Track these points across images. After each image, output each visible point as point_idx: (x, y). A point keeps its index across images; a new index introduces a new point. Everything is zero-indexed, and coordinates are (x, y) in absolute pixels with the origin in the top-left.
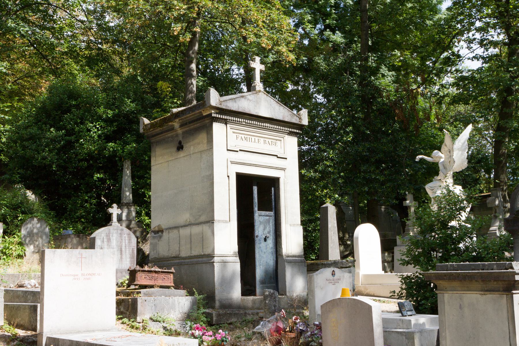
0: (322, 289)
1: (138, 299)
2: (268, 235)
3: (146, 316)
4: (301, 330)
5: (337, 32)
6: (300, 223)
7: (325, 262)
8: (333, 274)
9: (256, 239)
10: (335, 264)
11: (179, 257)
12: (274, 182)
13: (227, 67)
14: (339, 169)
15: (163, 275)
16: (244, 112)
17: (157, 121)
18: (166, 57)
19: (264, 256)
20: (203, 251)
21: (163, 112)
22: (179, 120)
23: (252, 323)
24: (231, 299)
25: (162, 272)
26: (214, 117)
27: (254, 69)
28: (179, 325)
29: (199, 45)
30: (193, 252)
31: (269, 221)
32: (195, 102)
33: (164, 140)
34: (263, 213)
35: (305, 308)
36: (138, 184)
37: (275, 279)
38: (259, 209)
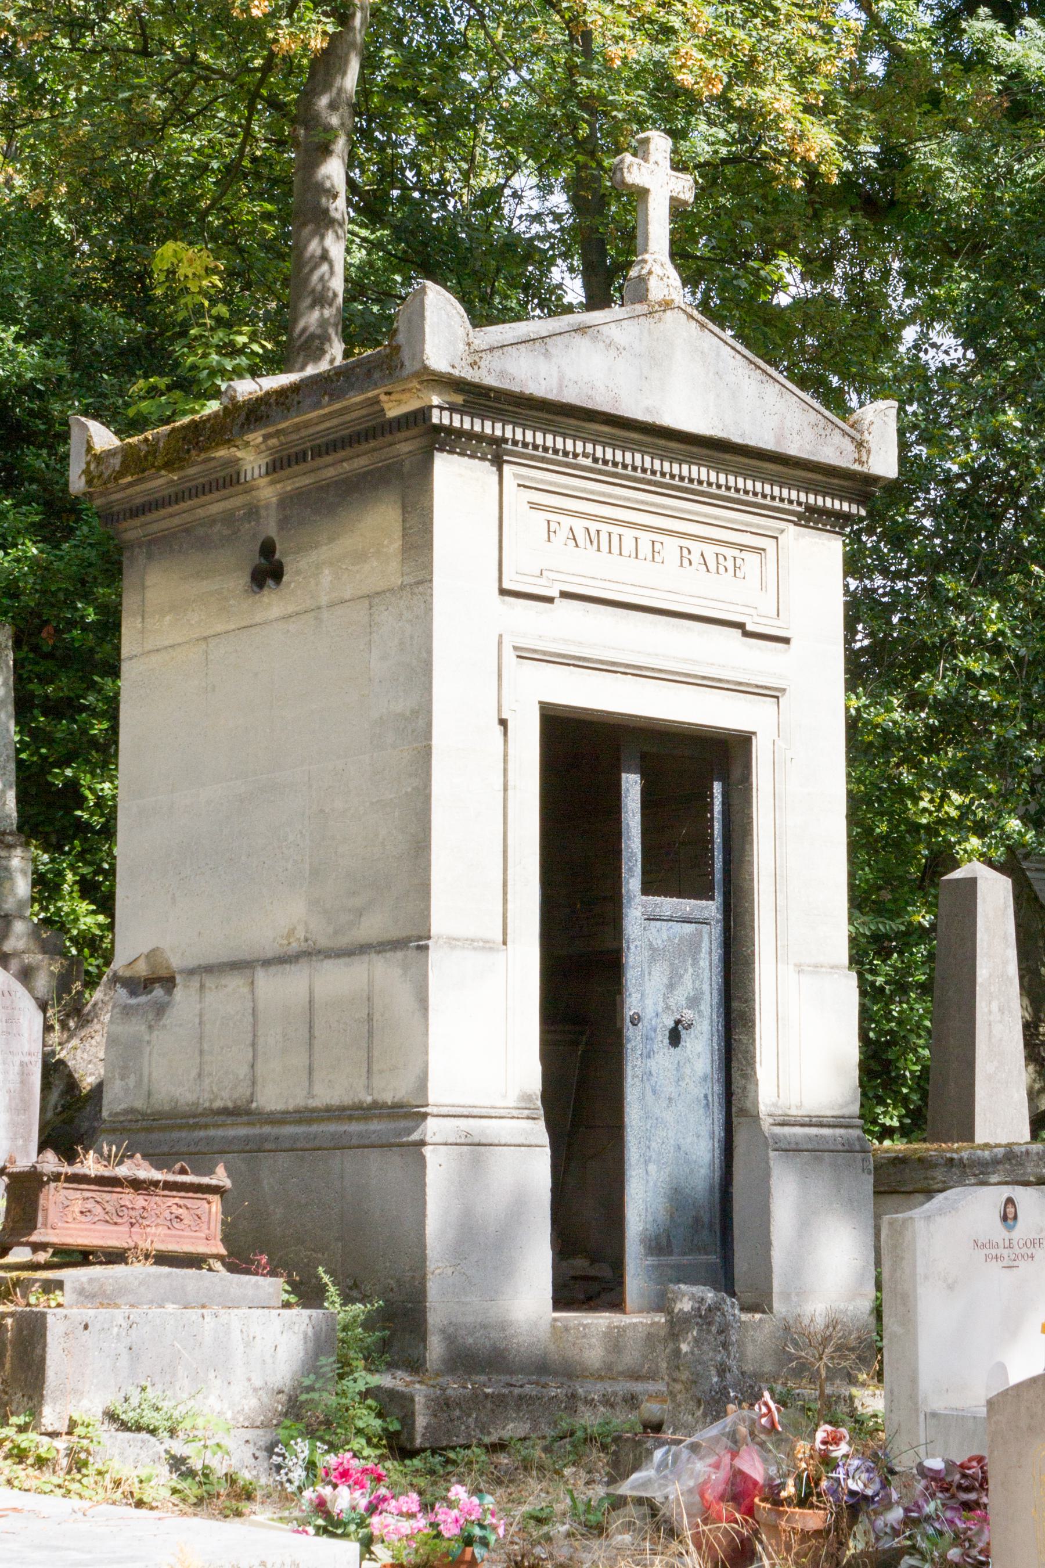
0: (951, 1287)
1: (50, 1320)
2: (688, 1015)
3: (85, 1403)
4: (852, 1493)
5: (1028, 22)
6: (845, 960)
7: (957, 1150)
8: (1009, 1216)
9: (629, 1031)
10: (1007, 1166)
11: (248, 1112)
12: (722, 756)
13: (488, 179)
14: (1027, 696)
15: (171, 1202)
16: (590, 405)
17: (157, 439)
18: (189, 122)
19: (669, 1116)
20: (368, 1087)
21: (177, 394)
22: (266, 437)
23: (604, 1448)
24: (503, 1326)
25: (169, 1186)
26: (439, 428)
27: (643, 193)
28: (249, 1451)
29: (362, 67)
30: (319, 1089)
31: (693, 946)
32: (336, 349)
33: (187, 531)
34: (668, 904)
35: (863, 1377)
36: (50, 741)
37: (718, 1234)
38: (649, 888)
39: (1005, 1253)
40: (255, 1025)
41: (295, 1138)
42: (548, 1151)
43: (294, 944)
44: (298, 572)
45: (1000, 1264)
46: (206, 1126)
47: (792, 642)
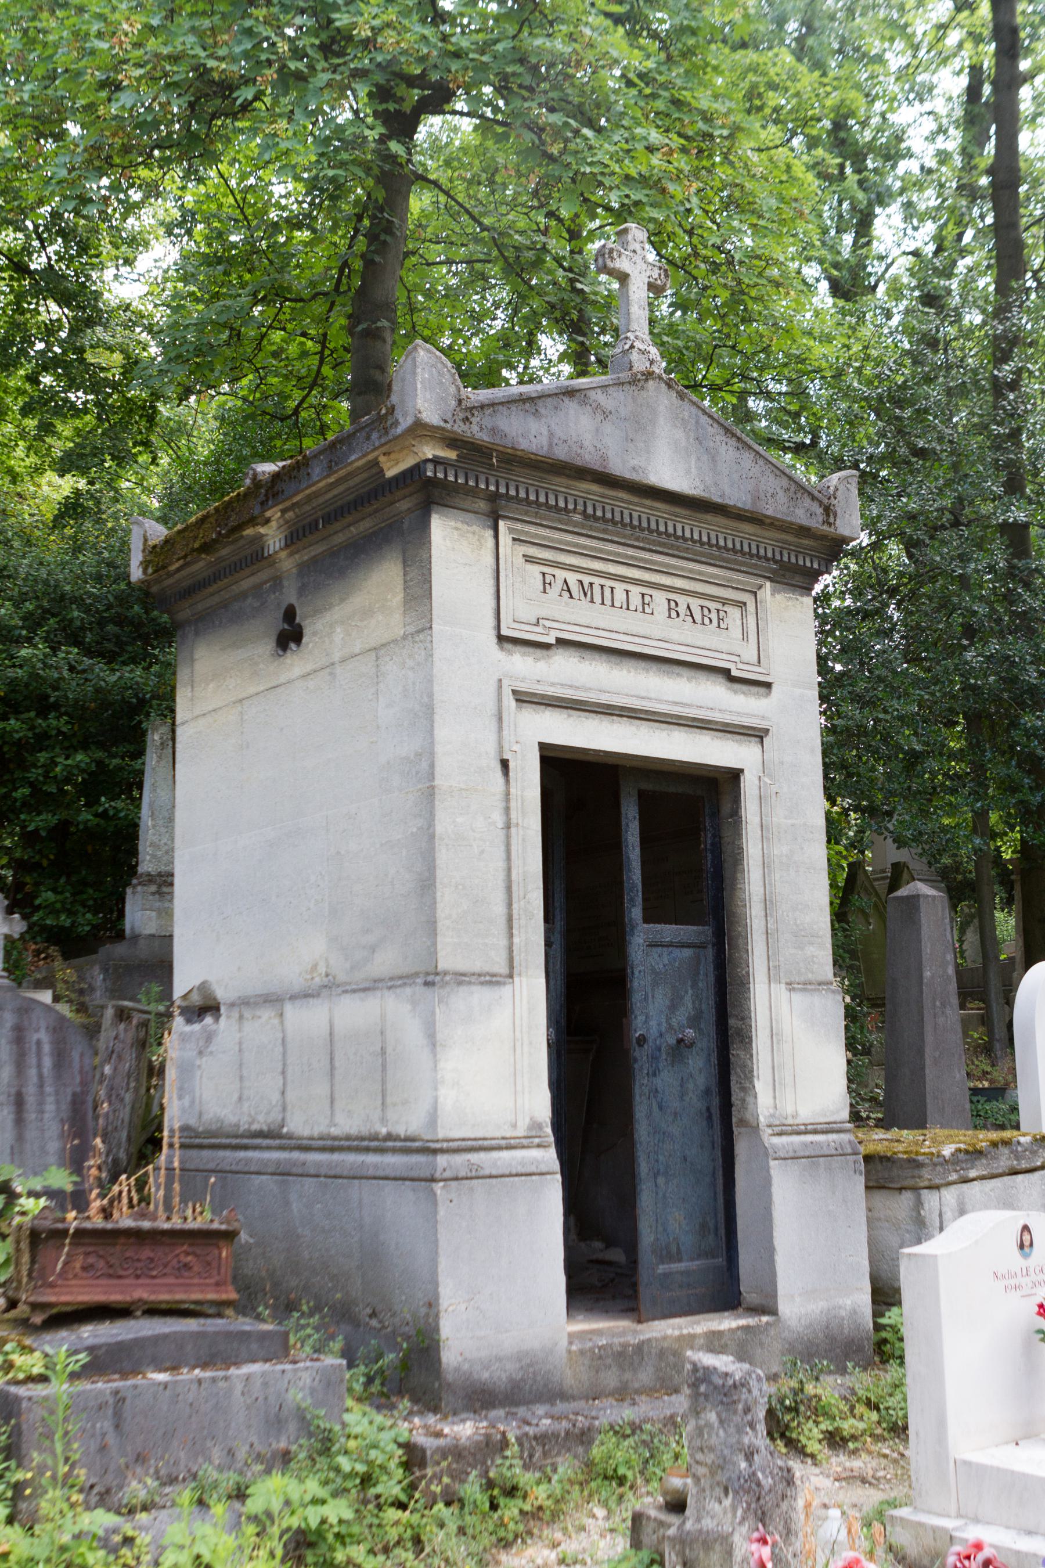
11: (280, 1136)
12: (718, 787)
16: (579, 462)
22: (284, 511)
34: (669, 931)
39: (1024, 1281)
40: (284, 1054)
41: (318, 1164)
42: (559, 1177)
43: (317, 980)
44: (315, 634)
45: (1019, 1293)
46: (245, 1147)
47: (774, 687)
